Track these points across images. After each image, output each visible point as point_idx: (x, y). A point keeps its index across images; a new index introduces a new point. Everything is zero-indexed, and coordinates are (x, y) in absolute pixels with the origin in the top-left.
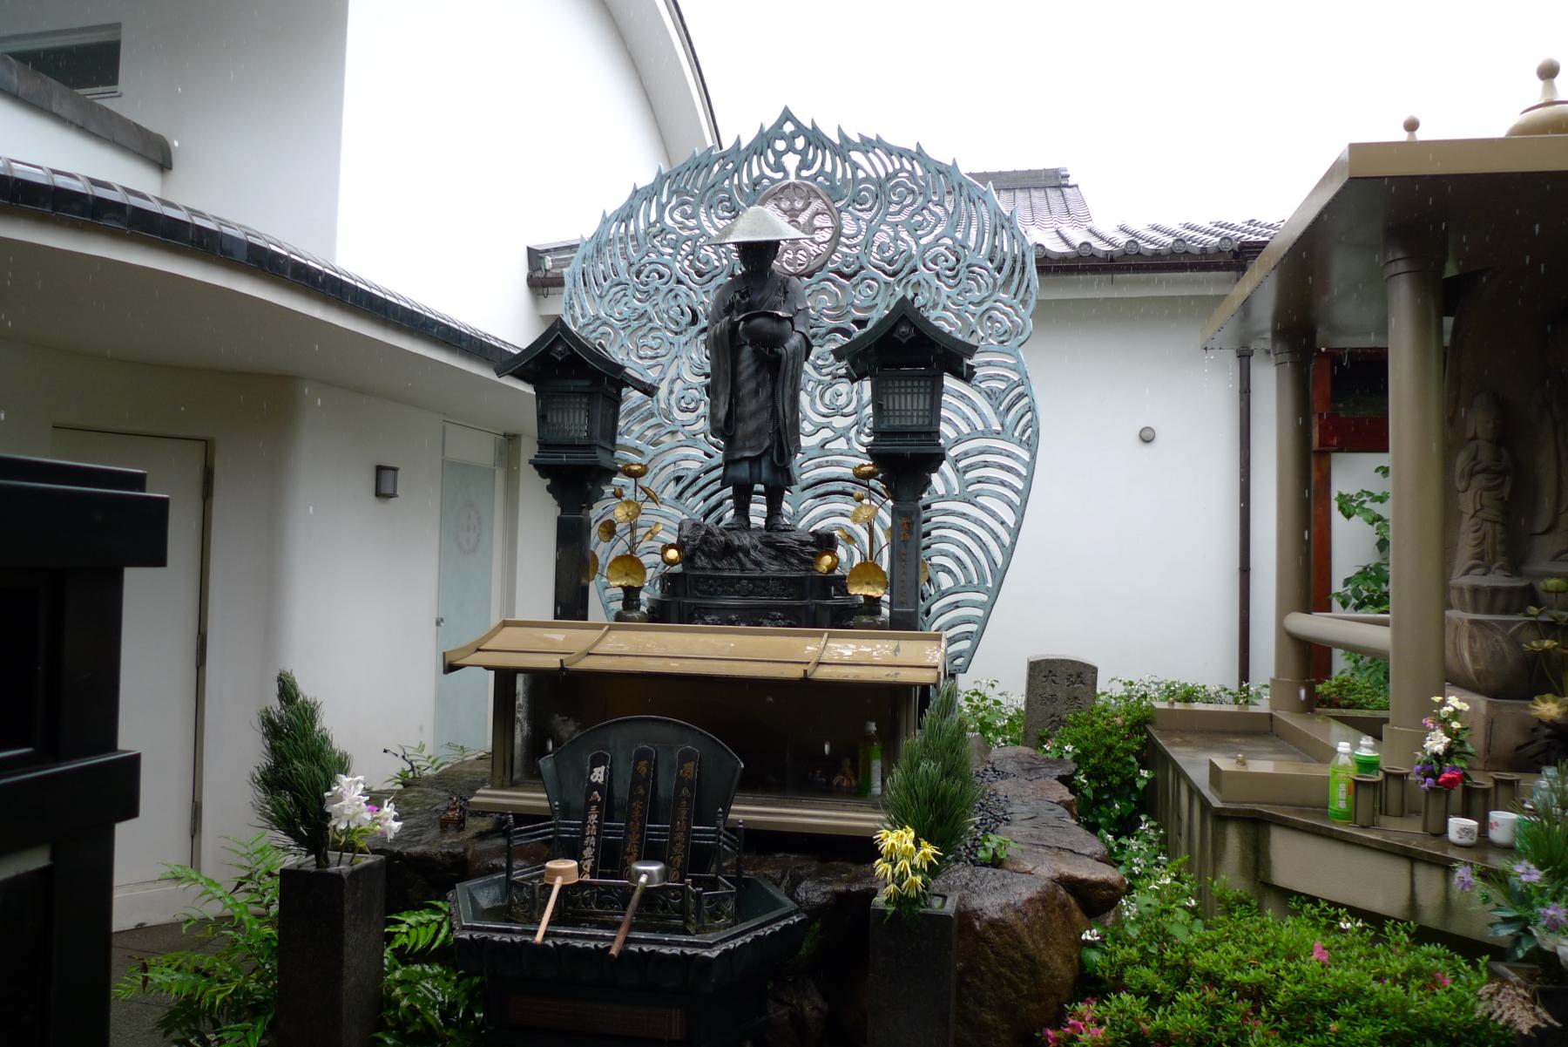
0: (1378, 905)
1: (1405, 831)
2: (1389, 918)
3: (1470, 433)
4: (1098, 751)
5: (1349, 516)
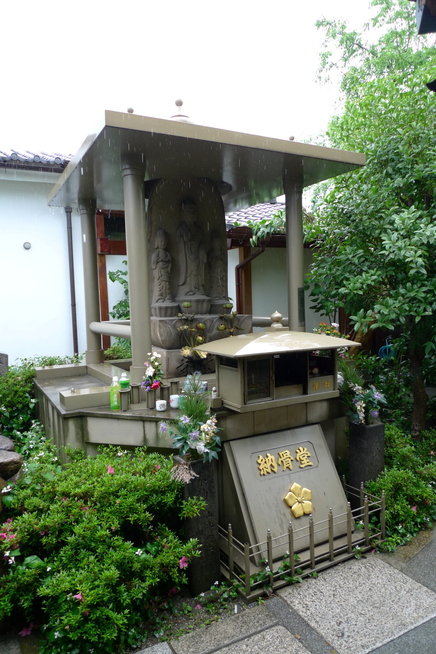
0: (131, 442)
1: (140, 409)
2: (136, 447)
3: (156, 246)
4: (9, 394)
5: (113, 281)
